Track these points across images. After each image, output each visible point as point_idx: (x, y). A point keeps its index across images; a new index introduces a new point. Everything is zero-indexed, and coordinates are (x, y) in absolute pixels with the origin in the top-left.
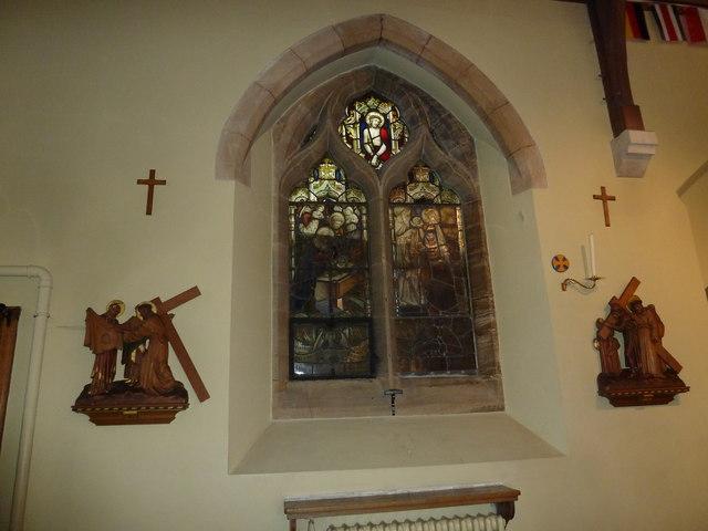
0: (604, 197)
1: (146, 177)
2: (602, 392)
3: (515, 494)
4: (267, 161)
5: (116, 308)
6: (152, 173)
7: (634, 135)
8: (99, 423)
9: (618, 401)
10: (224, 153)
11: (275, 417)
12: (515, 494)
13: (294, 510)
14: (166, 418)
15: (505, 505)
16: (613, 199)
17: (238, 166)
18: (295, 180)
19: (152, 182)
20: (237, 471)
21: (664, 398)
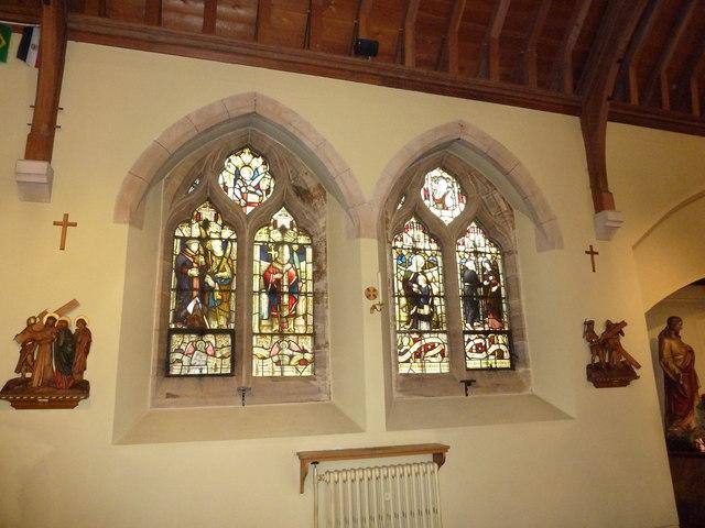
0: (592, 253)
1: (61, 219)
2: (589, 378)
3: (446, 448)
4: (159, 207)
5: (623, 335)
6: (66, 216)
7: (610, 214)
8: (17, 407)
9: (598, 384)
10: (121, 203)
11: (153, 405)
12: (446, 448)
13: (309, 460)
14: (71, 404)
15: (439, 456)
16: (597, 253)
17: (134, 212)
18: (173, 226)
19: (65, 224)
20: (121, 443)
21: (624, 383)
